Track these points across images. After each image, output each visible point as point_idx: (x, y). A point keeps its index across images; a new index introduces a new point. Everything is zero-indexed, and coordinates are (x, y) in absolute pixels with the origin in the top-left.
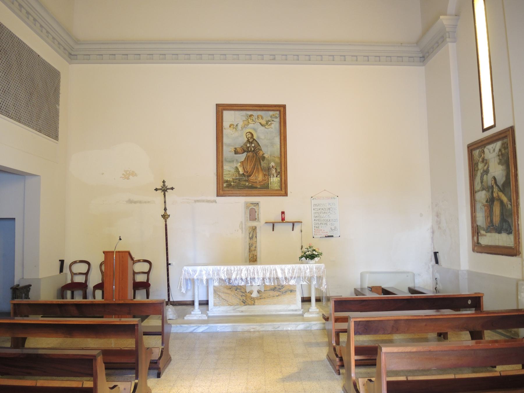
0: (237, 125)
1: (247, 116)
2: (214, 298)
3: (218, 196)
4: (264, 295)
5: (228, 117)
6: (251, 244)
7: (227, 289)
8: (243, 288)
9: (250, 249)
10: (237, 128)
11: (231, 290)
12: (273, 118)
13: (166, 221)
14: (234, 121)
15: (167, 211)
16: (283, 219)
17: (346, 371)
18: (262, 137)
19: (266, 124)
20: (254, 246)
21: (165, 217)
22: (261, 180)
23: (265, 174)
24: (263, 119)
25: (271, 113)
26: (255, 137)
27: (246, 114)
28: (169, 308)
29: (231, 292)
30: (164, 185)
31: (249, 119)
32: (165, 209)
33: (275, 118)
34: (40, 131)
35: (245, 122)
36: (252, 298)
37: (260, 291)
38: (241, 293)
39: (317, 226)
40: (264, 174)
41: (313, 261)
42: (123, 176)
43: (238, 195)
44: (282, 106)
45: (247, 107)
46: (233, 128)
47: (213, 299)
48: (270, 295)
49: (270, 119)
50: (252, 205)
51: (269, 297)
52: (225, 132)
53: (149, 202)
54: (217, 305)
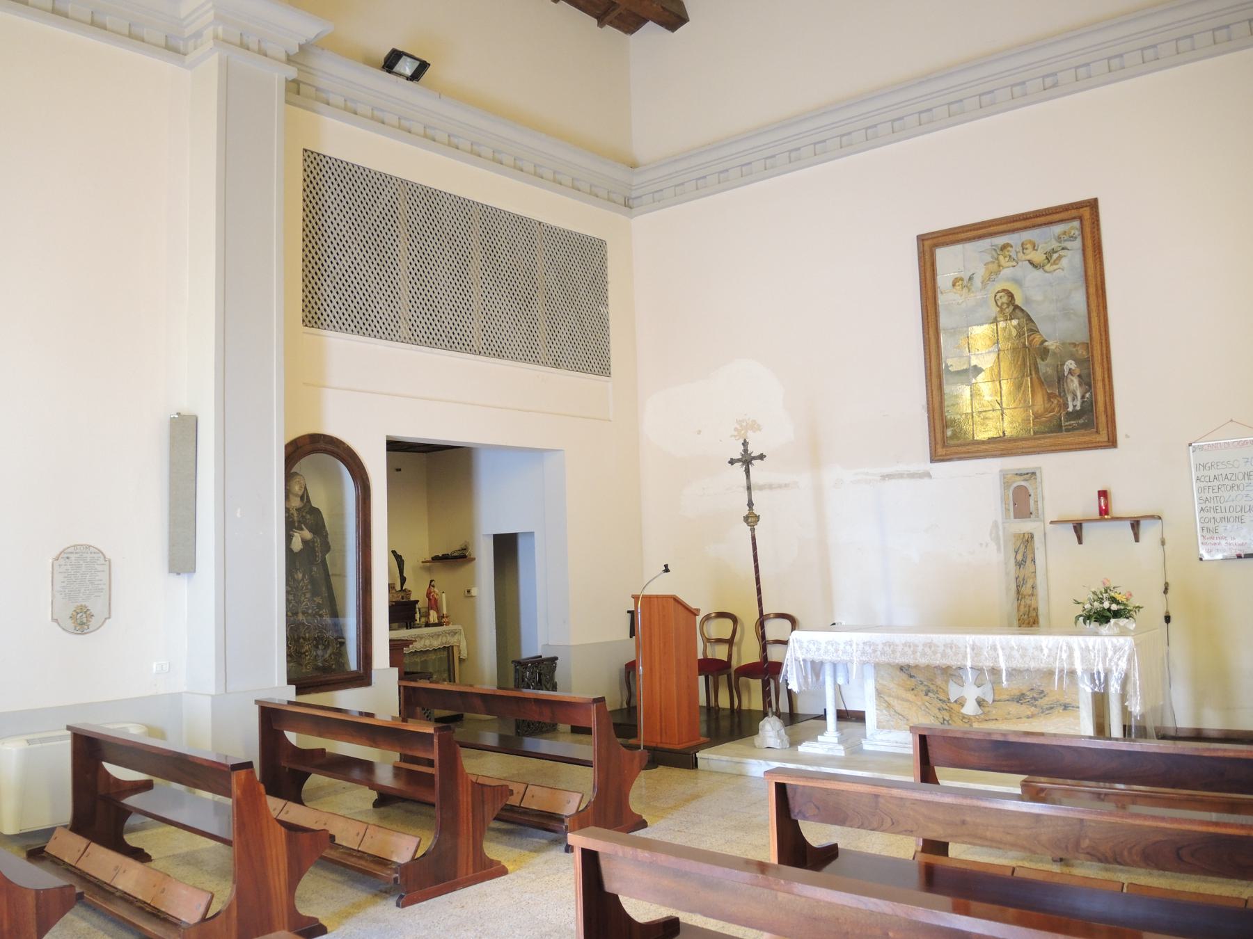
0: (971, 279)
1: (995, 250)
2: (877, 709)
3: (933, 460)
4: (994, 712)
5: (949, 261)
6: (1021, 579)
7: (906, 691)
8: (943, 690)
9: (1018, 592)
10: (972, 284)
11: (915, 692)
12: (1065, 241)
13: (753, 530)
14: (962, 269)
15: (754, 508)
16: (1104, 512)
17: (233, 802)
18: (1037, 296)
19: (1047, 261)
20: (1029, 585)
21: (751, 519)
22: (1040, 412)
23: (1051, 393)
24: (1037, 250)
25: (1058, 229)
26: (1018, 301)
27: (992, 246)
28: (769, 722)
29: (913, 697)
30: (746, 451)
31: (1001, 258)
32: (750, 504)
33: (1071, 241)
34: (556, 365)
35: (990, 266)
36: (964, 718)
37: (984, 700)
38: (939, 702)
39: (1211, 526)
40: (1048, 394)
41: (1105, 629)
42: (736, 433)
43: (982, 454)
44: (1085, 205)
45: (992, 228)
46: (962, 288)
47: (875, 711)
48: (1009, 714)
49: (1055, 245)
50: (1018, 478)
51: (1008, 717)
52: (942, 300)
53: (786, 485)
54: (884, 728)
